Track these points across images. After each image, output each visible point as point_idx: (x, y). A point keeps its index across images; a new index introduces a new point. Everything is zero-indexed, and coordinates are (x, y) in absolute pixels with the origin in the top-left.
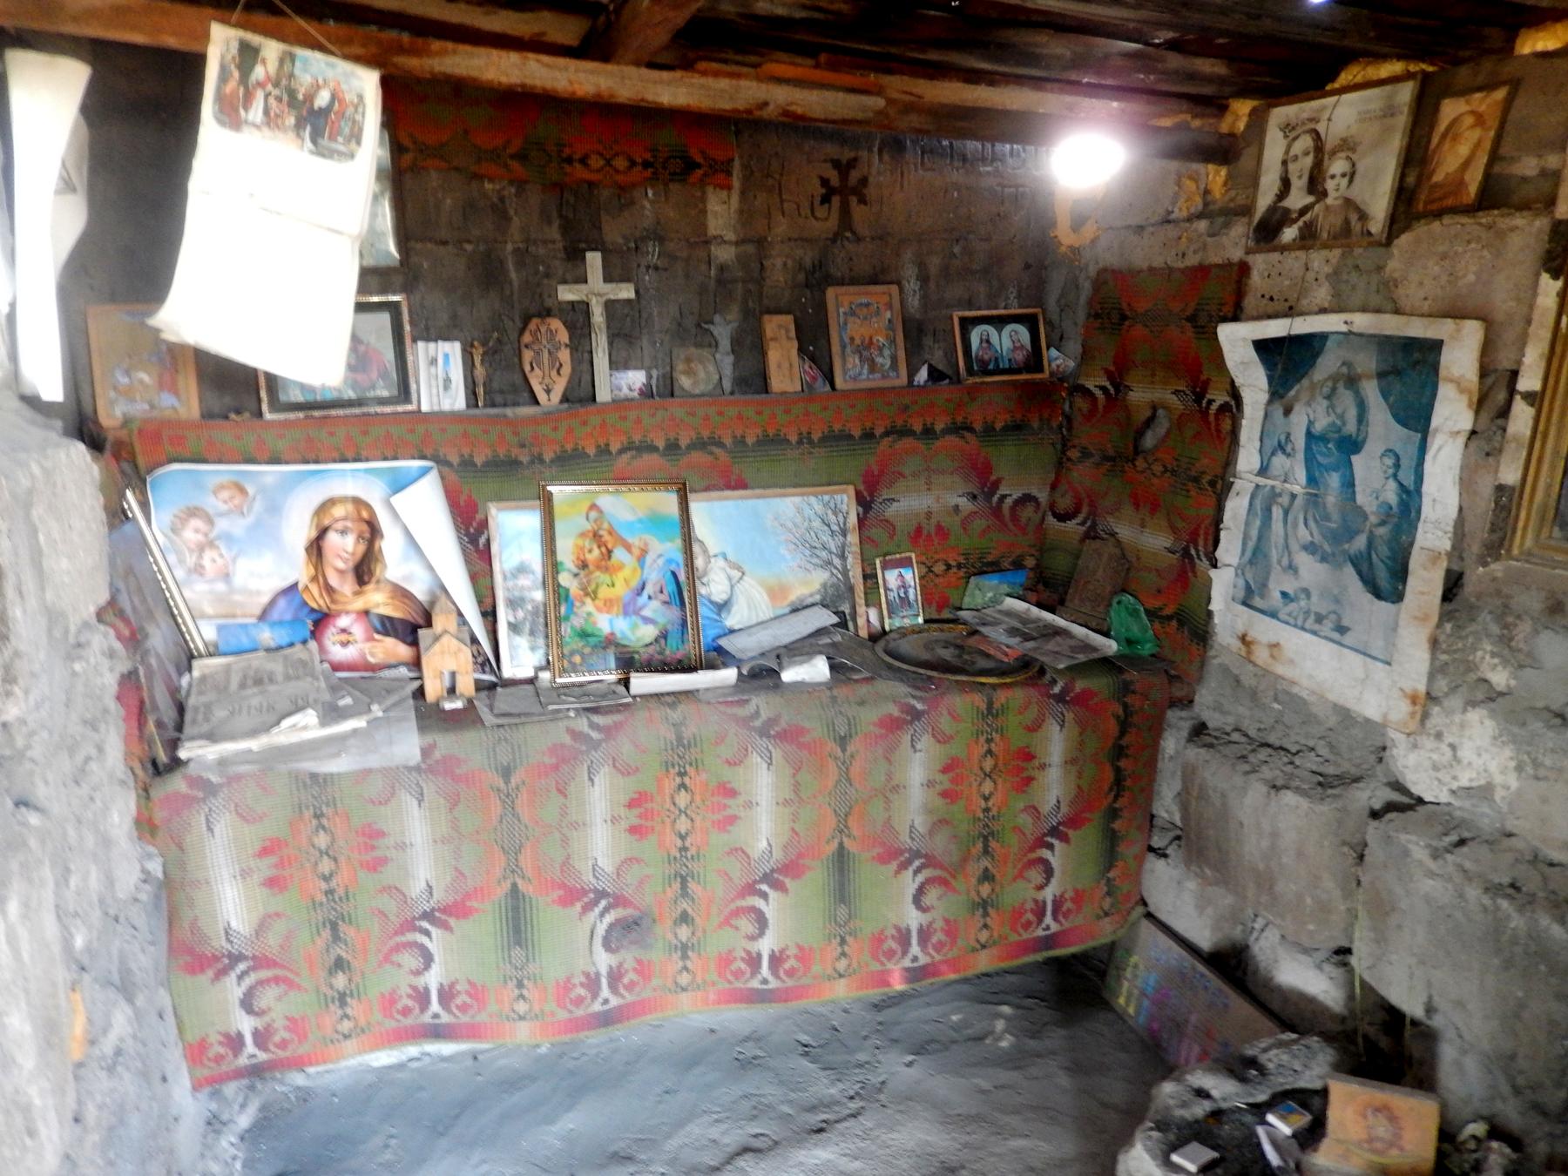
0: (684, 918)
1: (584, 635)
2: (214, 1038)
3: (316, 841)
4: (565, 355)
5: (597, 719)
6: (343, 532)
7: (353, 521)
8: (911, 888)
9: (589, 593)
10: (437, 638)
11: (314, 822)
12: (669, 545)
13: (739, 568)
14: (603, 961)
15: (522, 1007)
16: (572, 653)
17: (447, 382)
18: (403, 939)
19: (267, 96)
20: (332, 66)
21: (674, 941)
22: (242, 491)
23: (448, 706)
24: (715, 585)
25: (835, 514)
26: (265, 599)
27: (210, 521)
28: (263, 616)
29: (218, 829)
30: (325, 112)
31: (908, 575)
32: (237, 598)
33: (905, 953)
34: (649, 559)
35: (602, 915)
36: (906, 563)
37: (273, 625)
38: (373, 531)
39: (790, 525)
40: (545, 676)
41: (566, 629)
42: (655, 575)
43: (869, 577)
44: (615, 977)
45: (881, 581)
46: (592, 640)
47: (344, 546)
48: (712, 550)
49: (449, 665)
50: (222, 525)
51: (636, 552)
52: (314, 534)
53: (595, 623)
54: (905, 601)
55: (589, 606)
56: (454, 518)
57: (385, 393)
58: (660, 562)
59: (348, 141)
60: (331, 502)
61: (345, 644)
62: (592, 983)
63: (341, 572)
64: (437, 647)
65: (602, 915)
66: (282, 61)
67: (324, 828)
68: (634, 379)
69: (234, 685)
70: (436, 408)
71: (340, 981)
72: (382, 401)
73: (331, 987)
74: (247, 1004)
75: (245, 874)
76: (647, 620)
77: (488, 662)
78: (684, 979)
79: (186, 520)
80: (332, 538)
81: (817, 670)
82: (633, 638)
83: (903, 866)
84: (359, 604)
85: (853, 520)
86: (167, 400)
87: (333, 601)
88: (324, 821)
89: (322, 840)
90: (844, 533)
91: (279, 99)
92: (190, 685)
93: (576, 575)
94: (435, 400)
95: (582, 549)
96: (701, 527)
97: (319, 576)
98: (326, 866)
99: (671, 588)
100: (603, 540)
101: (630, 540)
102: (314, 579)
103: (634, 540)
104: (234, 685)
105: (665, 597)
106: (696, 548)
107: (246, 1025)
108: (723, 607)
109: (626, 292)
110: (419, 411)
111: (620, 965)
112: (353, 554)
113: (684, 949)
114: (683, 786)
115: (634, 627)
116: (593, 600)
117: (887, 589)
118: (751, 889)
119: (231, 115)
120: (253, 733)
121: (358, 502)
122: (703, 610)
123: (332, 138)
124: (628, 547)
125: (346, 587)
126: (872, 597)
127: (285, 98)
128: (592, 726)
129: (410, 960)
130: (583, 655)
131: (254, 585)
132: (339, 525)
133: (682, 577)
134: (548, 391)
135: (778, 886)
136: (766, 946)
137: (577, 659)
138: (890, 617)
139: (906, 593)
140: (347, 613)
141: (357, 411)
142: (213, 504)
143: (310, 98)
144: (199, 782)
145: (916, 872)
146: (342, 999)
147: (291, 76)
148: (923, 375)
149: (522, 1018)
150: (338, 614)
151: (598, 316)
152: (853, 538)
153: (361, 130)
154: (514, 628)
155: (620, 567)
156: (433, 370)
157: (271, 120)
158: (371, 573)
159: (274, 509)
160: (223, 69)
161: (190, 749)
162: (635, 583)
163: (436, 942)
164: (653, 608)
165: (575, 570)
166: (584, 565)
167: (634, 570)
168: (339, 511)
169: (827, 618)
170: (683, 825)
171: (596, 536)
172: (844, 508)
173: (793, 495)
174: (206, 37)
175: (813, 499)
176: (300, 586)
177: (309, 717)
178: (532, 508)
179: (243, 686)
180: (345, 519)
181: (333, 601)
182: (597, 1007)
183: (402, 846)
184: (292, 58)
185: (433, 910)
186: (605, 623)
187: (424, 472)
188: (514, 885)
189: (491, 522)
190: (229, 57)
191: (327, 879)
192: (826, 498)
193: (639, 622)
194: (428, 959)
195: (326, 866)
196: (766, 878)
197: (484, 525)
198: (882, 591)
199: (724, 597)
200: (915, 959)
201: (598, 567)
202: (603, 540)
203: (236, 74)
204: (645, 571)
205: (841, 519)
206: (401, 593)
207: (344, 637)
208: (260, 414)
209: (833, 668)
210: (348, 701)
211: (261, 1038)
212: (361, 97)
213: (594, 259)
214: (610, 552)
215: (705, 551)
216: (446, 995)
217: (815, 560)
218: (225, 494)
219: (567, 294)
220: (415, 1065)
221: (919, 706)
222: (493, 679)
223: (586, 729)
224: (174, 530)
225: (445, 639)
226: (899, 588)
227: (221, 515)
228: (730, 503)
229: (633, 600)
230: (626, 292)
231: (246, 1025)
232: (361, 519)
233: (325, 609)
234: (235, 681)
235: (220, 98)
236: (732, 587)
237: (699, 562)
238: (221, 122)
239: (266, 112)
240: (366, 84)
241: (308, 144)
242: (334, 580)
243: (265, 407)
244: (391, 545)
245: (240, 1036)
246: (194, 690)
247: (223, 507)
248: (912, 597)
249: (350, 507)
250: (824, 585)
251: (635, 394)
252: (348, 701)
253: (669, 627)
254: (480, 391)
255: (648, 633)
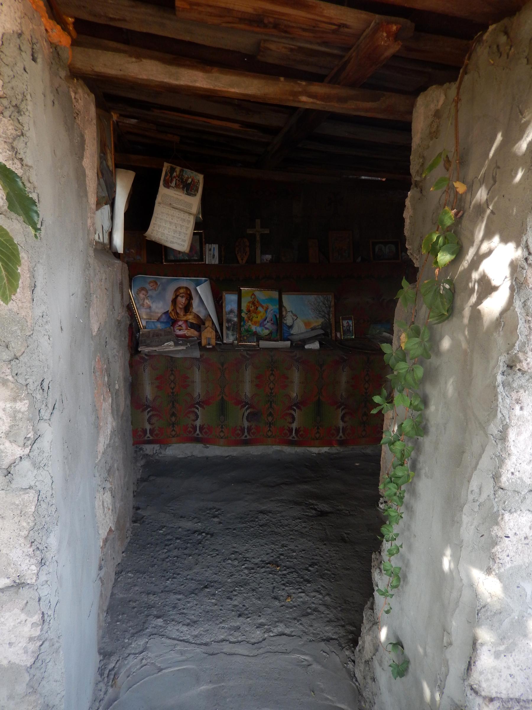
0: (270, 414)
1: (247, 331)
2: (140, 429)
3: (170, 377)
4: (247, 249)
5: (249, 352)
6: (182, 297)
7: (185, 294)
8: (341, 415)
9: (250, 319)
10: (206, 328)
11: (171, 372)
12: (275, 307)
13: (296, 316)
14: (246, 424)
15: (222, 434)
16: (244, 336)
17: (214, 255)
18: (190, 410)
19: (176, 180)
20: (192, 173)
21: (267, 421)
22: (156, 283)
23: (208, 347)
24: (288, 321)
25: (327, 301)
26: (159, 315)
27: (147, 292)
28: (159, 320)
29: (146, 371)
30: (190, 184)
31: (350, 323)
32: (152, 314)
33: (338, 435)
34: (268, 311)
35: (247, 409)
36: (350, 319)
37: (161, 322)
38: (190, 298)
39: (312, 303)
40: (236, 342)
41: (243, 329)
42: (269, 316)
43: (337, 323)
44: (249, 429)
45: (341, 324)
46: (250, 333)
47: (182, 301)
48: (288, 310)
49: (209, 335)
50: (150, 293)
51: (265, 308)
52: (174, 297)
53: (251, 328)
54: (349, 330)
55: (250, 323)
56: (214, 300)
57: (196, 258)
58: (272, 312)
59: (195, 191)
60: (179, 288)
61: (180, 330)
62: (242, 430)
63: (180, 308)
64: (206, 330)
65: (247, 409)
66: (180, 172)
67: (173, 374)
68: (268, 257)
69: (151, 336)
70: (210, 263)
71: (173, 419)
72: (195, 261)
73: (171, 420)
74: (149, 421)
75: (152, 383)
76: (267, 328)
77: (219, 337)
78: (269, 434)
79: (141, 291)
80: (179, 298)
81: (316, 346)
82: (262, 333)
83: (339, 407)
84: (185, 318)
85: (333, 303)
86: (138, 257)
87: (178, 317)
88: (173, 372)
89: (172, 378)
90: (330, 307)
91: (179, 181)
92: (139, 336)
93: (247, 314)
94: (210, 261)
95: (249, 306)
96: (285, 303)
97: (174, 309)
98: (172, 385)
99: (274, 319)
100: (255, 303)
101: (263, 305)
102: (173, 310)
103: (264, 305)
104: (151, 336)
105: (272, 322)
106: (283, 309)
107: (148, 427)
108: (291, 327)
109: (267, 231)
110: (205, 264)
111: (251, 426)
112: (184, 303)
113: (270, 424)
114: (272, 374)
115: (263, 330)
116: (251, 321)
117: (343, 326)
118: (290, 408)
119: (167, 185)
120: (157, 346)
121: (187, 288)
122: (285, 328)
123: (191, 191)
124: (262, 307)
125: (182, 313)
126: (337, 329)
127: (181, 180)
128: (247, 354)
129: (192, 417)
130: (247, 337)
131: (157, 310)
132: (181, 295)
133: (278, 317)
134: (242, 260)
135: (299, 408)
136: (294, 426)
137: (245, 338)
138: (343, 335)
139: (349, 328)
140: (182, 321)
141: (188, 263)
142: (148, 287)
143: (187, 180)
144: (142, 358)
145: (342, 410)
146: (173, 424)
147: (182, 175)
148: (359, 259)
149: (222, 438)
150: (179, 321)
151: (258, 238)
152: (332, 309)
153: (198, 189)
154: (228, 328)
155: (260, 312)
156: (210, 252)
157: (177, 186)
158: (189, 310)
159: (164, 289)
160: (166, 173)
161: (142, 348)
162: (264, 317)
163: (199, 412)
164: (268, 325)
165: (247, 312)
166: (249, 311)
167: (264, 314)
168: (182, 291)
169: (322, 332)
170: (272, 386)
171: (253, 303)
172: (331, 299)
173: (314, 295)
174: (163, 166)
175: (320, 296)
176: (169, 312)
177: (172, 343)
178: (235, 294)
179: (153, 336)
180: (183, 293)
181: (178, 317)
182: (243, 438)
183: (193, 382)
184: (183, 171)
185: (200, 402)
186: (254, 328)
187: (206, 281)
188: (222, 397)
189: (223, 297)
190: (168, 170)
191: (173, 389)
192: (325, 296)
193: (264, 329)
194: (197, 417)
195: (172, 385)
196: (295, 405)
197: (221, 298)
198: (341, 327)
199: (291, 324)
200: (341, 437)
201: (254, 312)
202: (255, 303)
203: (169, 174)
204: (267, 314)
205: (329, 303)
206: (197, 317)
207: (180, 328)
208: (162, 263)
209: (321, 344)
210: (181, 342)
211: (152, 431)
212: (199, 181)
213: (258, 221)
214: (257, 308)
215: (286, 310)
216: (201, 428)
217: (320, 315)
218: (152, 284)
219: (250, 231)
220: (190, 458)
221: (345, 358)
222: (221, 343)
223: (246, 355)
224: (138, 294)
225: (208, 328)
226: (347, 326)
227: (150, 290)
228: (294, 296)
229: (263, 322)
230: (267, 231)
231: (148, 427)
232: (188, 294)
233: (175, 319)
234: (151, 335)
235: (164, 180)
236: (294, 321)
237: (284, 313)
238: (165, 186)
239: (176, 184)
240: (200, 178)
241: (185, 192)
242: (178, 311)
243: (164, 261)
244: (195, 303)
245: (146, 430)
246: (141, 337)
247: (151, 288)
248: (351, 329)
249: (185, 290)
250: (322, 323)
251: (268, 262)
252: (181, 342)
253: (273, 331)
254: (223, 259)
255: (267, 332)
